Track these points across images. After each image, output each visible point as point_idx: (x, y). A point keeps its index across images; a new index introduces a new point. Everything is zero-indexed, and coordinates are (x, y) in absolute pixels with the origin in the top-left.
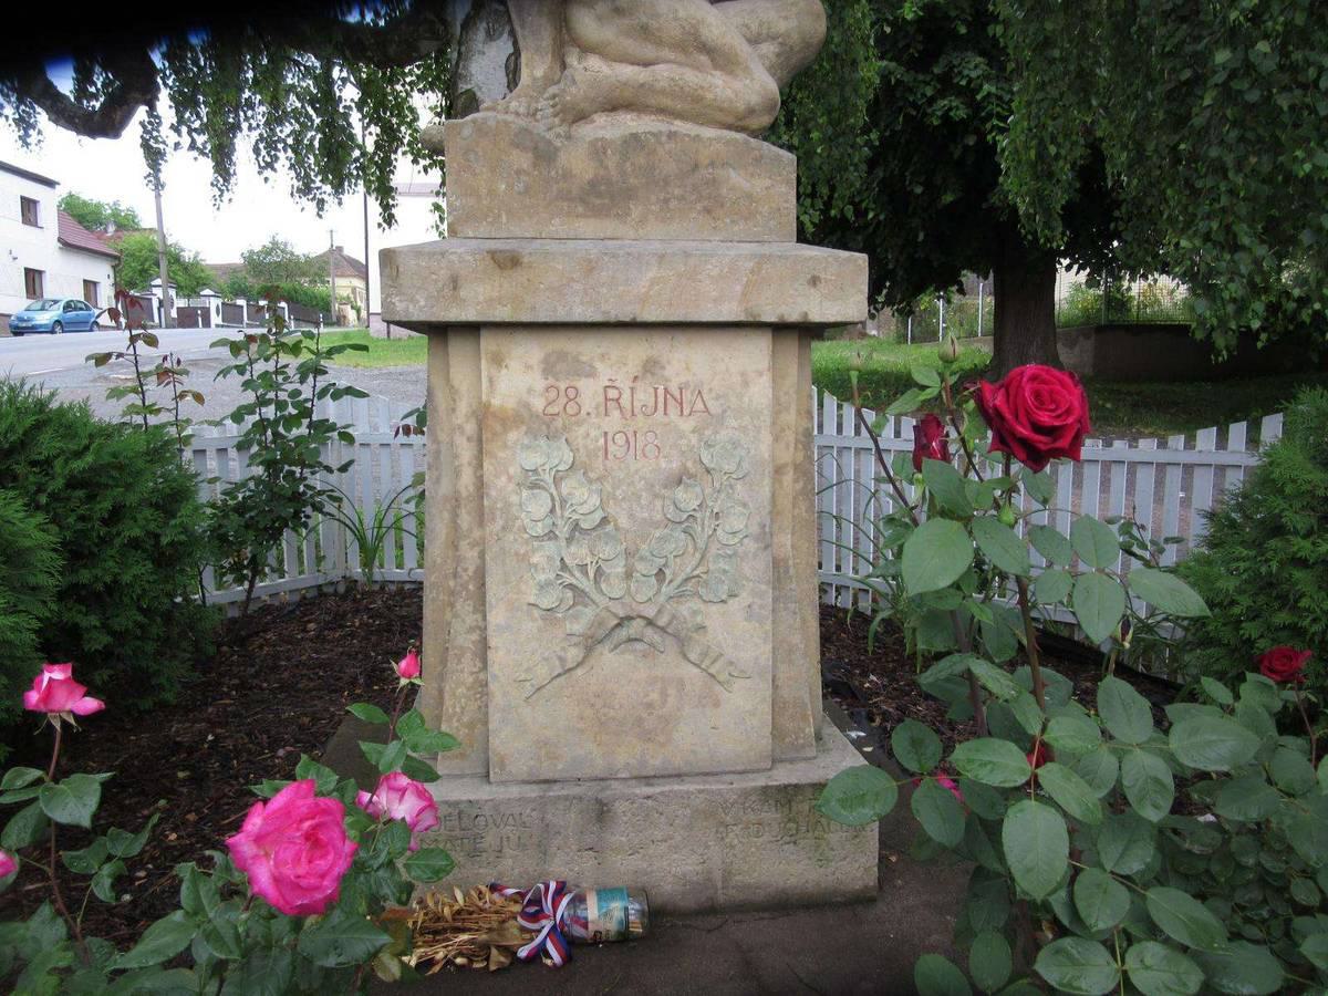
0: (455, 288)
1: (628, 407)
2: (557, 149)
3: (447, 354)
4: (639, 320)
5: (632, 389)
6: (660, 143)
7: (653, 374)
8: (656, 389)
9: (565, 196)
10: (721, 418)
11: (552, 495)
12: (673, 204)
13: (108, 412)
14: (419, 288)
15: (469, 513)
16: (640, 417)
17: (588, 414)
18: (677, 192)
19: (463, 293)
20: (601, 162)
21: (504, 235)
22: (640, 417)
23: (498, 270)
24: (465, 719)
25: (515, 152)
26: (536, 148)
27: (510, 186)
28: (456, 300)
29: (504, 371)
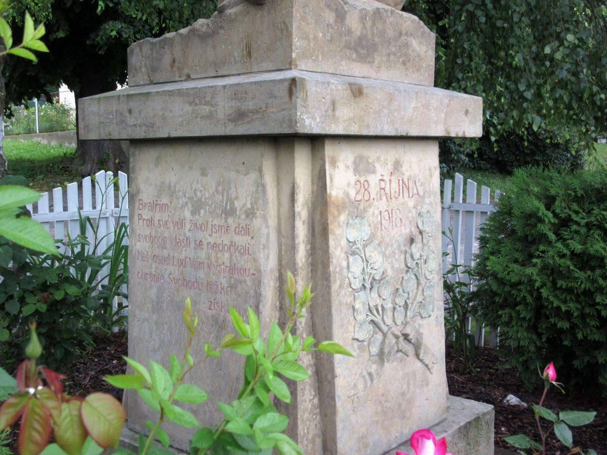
0: (334, 110)
1: (388, 193)
2: (346, 12)
3: (293, 157)
4: (409, 135)
5: (390, 180)
6: (388, 17)
7: (398, 171)
8: (399, 180)
9: (347, 46)
10: (424, 197)
11: (362, 257)
12: (392, 57)
13: (331, 269)
14: (317, 109)
15: (302, 280)
16: (394, 199)
17: (374, 199)
18: (393, 49)
19: (337, 113)
20: (364, 24)
21: (319, 71)
22: (394, 199)
23: (353, 97)
24: (310, 437)
25: (327, 11)
26: (337, 9)
27: (324, 36)
28: (335, 119)
29: (337, 170)
